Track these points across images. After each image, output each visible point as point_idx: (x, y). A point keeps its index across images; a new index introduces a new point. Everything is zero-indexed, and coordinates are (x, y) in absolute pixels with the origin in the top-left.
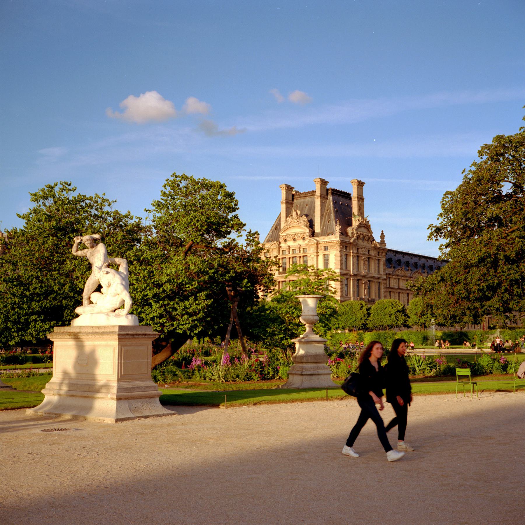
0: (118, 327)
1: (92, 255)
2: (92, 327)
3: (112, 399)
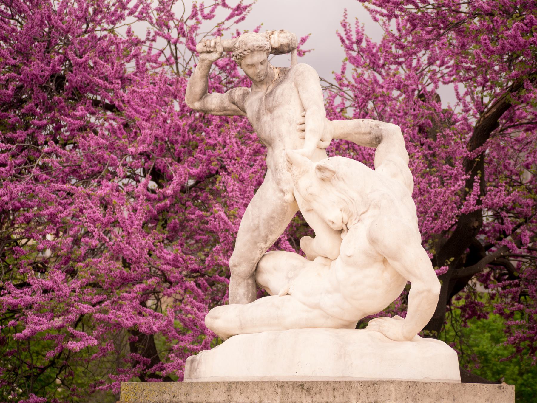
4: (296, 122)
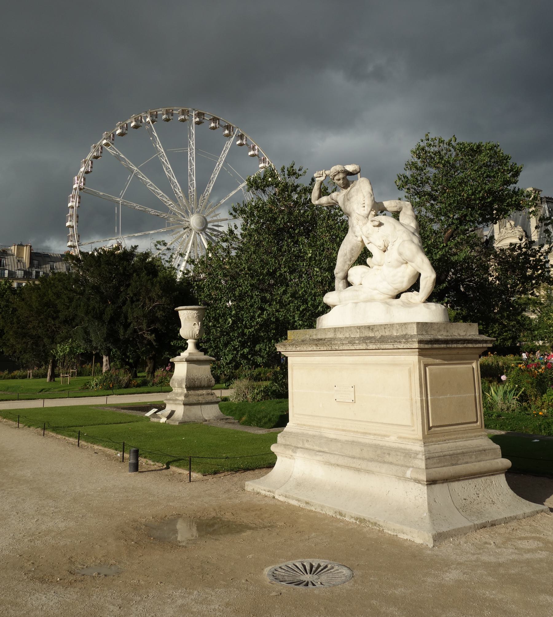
0: (415, 326)
1: (347, 199)
2: (359, 328)
3: (417, 481)
4: (357, 200)
